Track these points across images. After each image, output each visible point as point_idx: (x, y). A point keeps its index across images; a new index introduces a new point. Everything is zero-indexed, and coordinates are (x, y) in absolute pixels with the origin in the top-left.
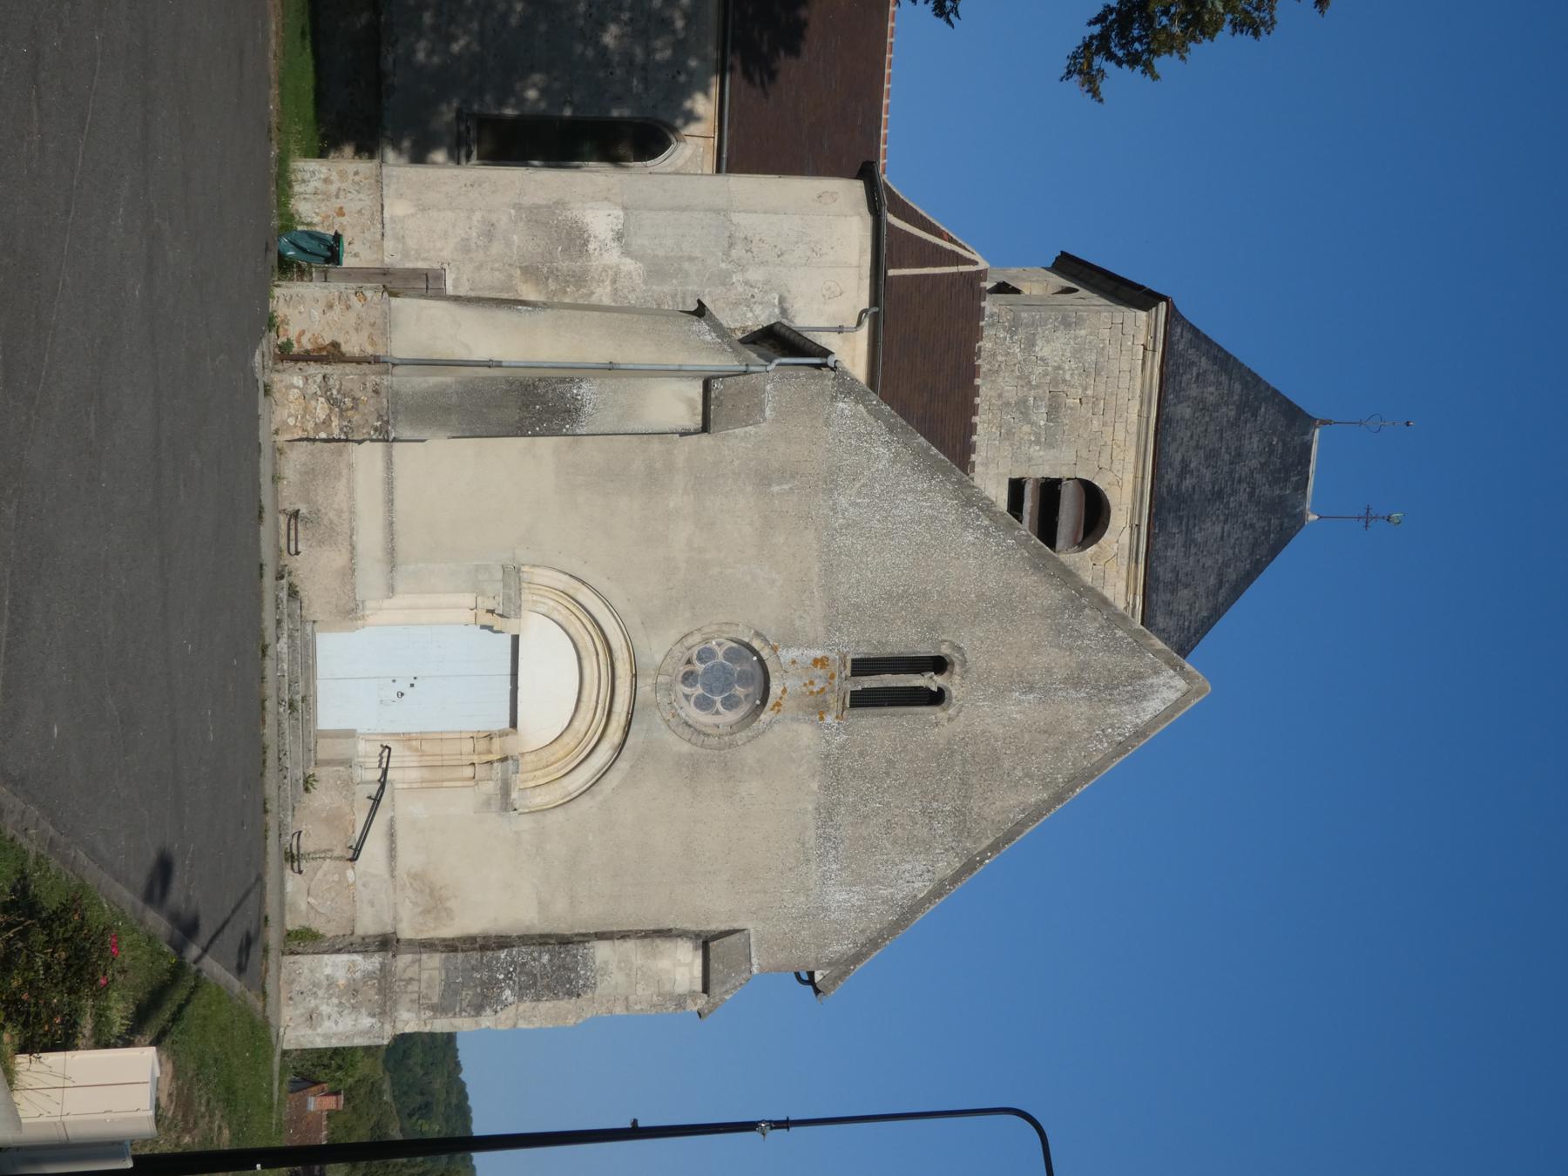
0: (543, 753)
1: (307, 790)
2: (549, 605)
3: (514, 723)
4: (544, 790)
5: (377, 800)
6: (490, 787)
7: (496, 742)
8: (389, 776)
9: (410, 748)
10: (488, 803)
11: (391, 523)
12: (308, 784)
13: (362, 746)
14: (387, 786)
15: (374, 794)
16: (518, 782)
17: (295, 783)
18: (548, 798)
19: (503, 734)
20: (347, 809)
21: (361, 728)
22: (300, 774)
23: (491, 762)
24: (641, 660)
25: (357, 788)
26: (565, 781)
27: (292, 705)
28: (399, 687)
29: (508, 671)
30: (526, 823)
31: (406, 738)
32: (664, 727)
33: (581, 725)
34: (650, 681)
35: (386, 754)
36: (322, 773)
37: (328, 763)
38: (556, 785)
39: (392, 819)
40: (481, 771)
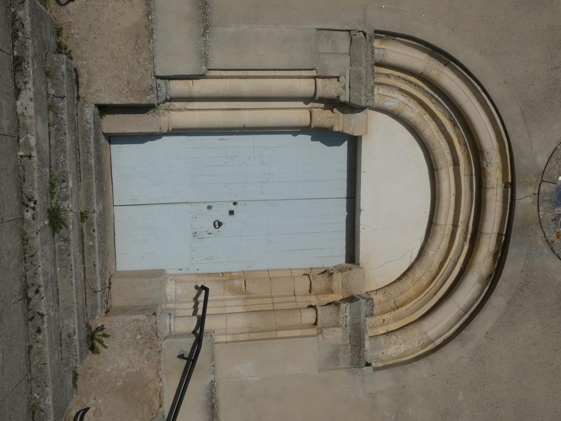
0: (392, 291)
1: (93, 348)
2: (395, 101)
3: (352, 256)
4: (400, 336)
5: (191, 360)
6: (337, 336)
7: (338, 278)
8: (209, 324)
9: (233, 290)
10: (334, 358)
11: (213, 407)
12: (93, 340)
13: (171, 289)
14: (205, 340)
15: (187, 351)
16: (374, 326)
17: (62, 340)
18: (403, 348)
19: (341, 270)
20: (151, 374)
21: (171, 268)
22: (73, 324)
23: (336, 304)
24: (521, 163)
25: (164, 344)
26: (427, 324)
27: (56, 220)
28: (221, 214)
29: (343, 192)
30: (383, 382)
31: (226, 278)
32: (546, 250)
33: (435, 254)
34: (531, 190)
35: (201, 298)
36: (114, 324)
37: (124, 310)
38: (415, 331)
39: (212, 386)
40: (325, 315)
